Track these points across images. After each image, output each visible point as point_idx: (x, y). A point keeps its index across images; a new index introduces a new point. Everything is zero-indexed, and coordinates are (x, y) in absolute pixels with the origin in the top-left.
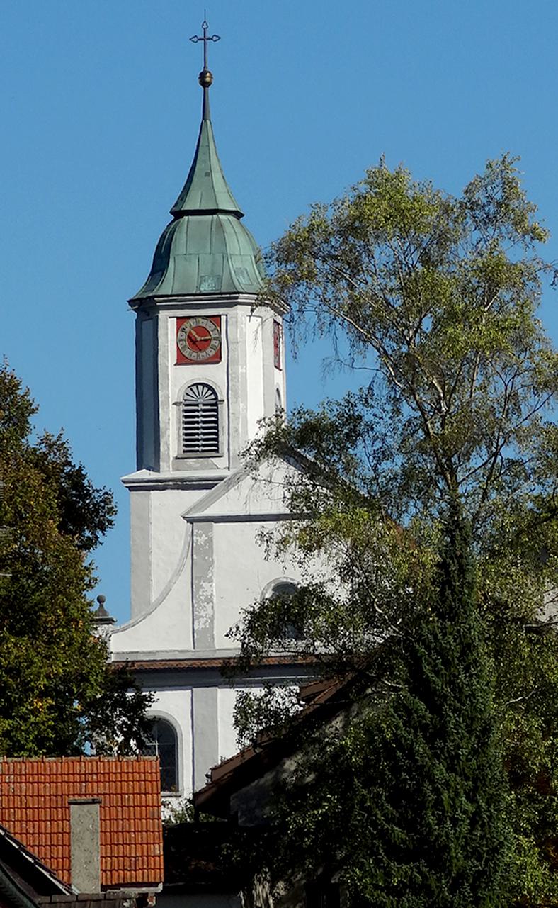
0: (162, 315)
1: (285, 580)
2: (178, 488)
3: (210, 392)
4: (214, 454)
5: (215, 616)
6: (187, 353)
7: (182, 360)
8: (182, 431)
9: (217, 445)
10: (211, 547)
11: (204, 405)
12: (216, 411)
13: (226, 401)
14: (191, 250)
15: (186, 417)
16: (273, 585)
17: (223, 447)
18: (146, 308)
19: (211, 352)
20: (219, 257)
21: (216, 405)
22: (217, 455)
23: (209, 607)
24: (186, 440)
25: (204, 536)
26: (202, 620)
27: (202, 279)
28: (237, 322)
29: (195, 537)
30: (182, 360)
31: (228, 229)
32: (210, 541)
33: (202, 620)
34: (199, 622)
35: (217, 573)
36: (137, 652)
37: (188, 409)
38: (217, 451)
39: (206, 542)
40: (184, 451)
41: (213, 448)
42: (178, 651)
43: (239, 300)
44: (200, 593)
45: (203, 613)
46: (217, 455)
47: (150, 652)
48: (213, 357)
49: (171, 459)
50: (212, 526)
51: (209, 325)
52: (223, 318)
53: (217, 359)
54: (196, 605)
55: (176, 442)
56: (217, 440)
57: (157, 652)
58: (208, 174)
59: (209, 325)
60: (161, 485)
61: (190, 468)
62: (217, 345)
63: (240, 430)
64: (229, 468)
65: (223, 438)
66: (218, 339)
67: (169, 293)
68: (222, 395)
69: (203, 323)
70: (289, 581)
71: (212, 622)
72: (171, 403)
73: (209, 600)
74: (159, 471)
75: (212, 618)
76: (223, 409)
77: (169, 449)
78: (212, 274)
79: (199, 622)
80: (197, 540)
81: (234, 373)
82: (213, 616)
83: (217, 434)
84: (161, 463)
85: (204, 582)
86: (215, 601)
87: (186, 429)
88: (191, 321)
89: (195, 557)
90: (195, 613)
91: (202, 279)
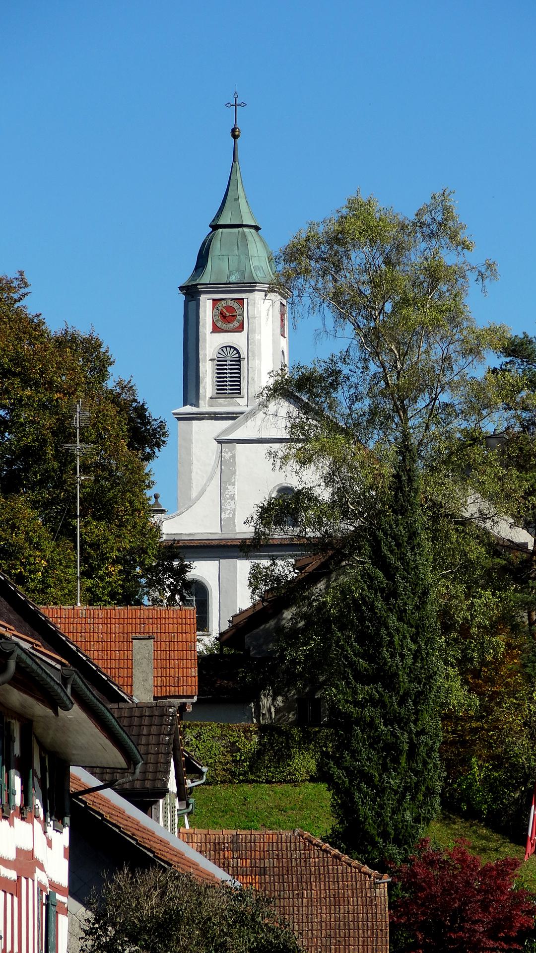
0: (203, 297)
1: (286, 485)
2: (212, 418)
3: (235, 352)
4: (237, 395)
5: (237, 510)
6: (219, 324)
7: (216, 329)
8: (215, 379)
9: (239, 389)
10: (234, 460)
11: (231, 361)
12: (239, 365)
13: (246, 359)
14: (223, 253)
15: (218, 369)
16: (277, 488)
17: (244, 391)
18: (191, 292)
19: (236, 324)
20: (243, 258)
21: (239, 361)
22: (240, 396)
23: (232, 502)
24: (218, 386)
25: (229, 453)
26: (227, 512)
27: (231, 273)
28: (254, 303)
29: (223, 454)
30: (216, 329)
31: (250, 238)
32: (234, 456)
33: (227, 512)
34: (225, 513)
35: (238, 479)
36: (182, 534)
37: (220, 364)
38: (240, 393)
39: (230, 457)
40: (217, 393)
41: (237, 391)
42: (210, 533)
43: (257, 288)
44: (226, 493)
45: (228, 507)
46: (240, 396)
47: (190, 534)
48: (237, 328)
49: (207, 398)
50: (235, 447)
51: (235, 305)
52: (245, 301)
53: (240, 329)
54: (223, 501)
55: (211, 386)
56: (239, 385)
57: (195, 534)
58: (237, 199)
59: (235, 305)
60: (200, 417)
61: (221, 405)
62: (240, 319)
63: (256, 379)
64: (247, 406)
65: (244, 384)
66: (242, 315)
67: (208, 282)
68: (244, 354)
69: (231, 303)
70: (289, 485)
71: (234, 514)
72: (208, 358)
73: (232, 498)
74: (198, 407)
75: (234, 511)
76: (244, 364)
77: (205, 391)
78: (238, 270)
79: (225, 513)
80: (225, 456)
81: (253, 339)
82: (235, 509)
83: (239, 381)
84: (200, 402)
85: (229, 485)
86: (236, 499)
87: (218, 378)
88: (222, 302)
89: (223, 467)
90: (222, 507)
91: (231, 273)
